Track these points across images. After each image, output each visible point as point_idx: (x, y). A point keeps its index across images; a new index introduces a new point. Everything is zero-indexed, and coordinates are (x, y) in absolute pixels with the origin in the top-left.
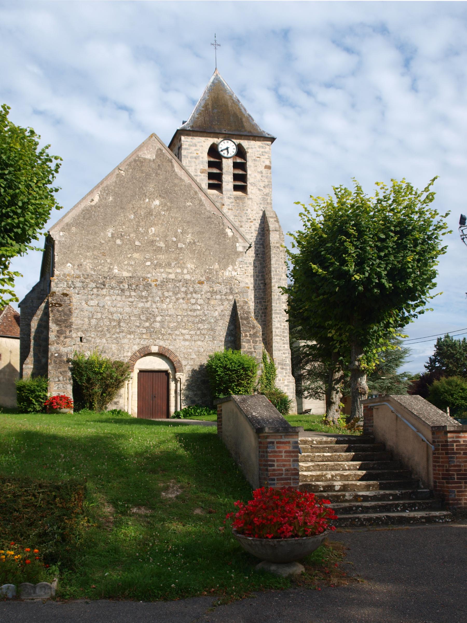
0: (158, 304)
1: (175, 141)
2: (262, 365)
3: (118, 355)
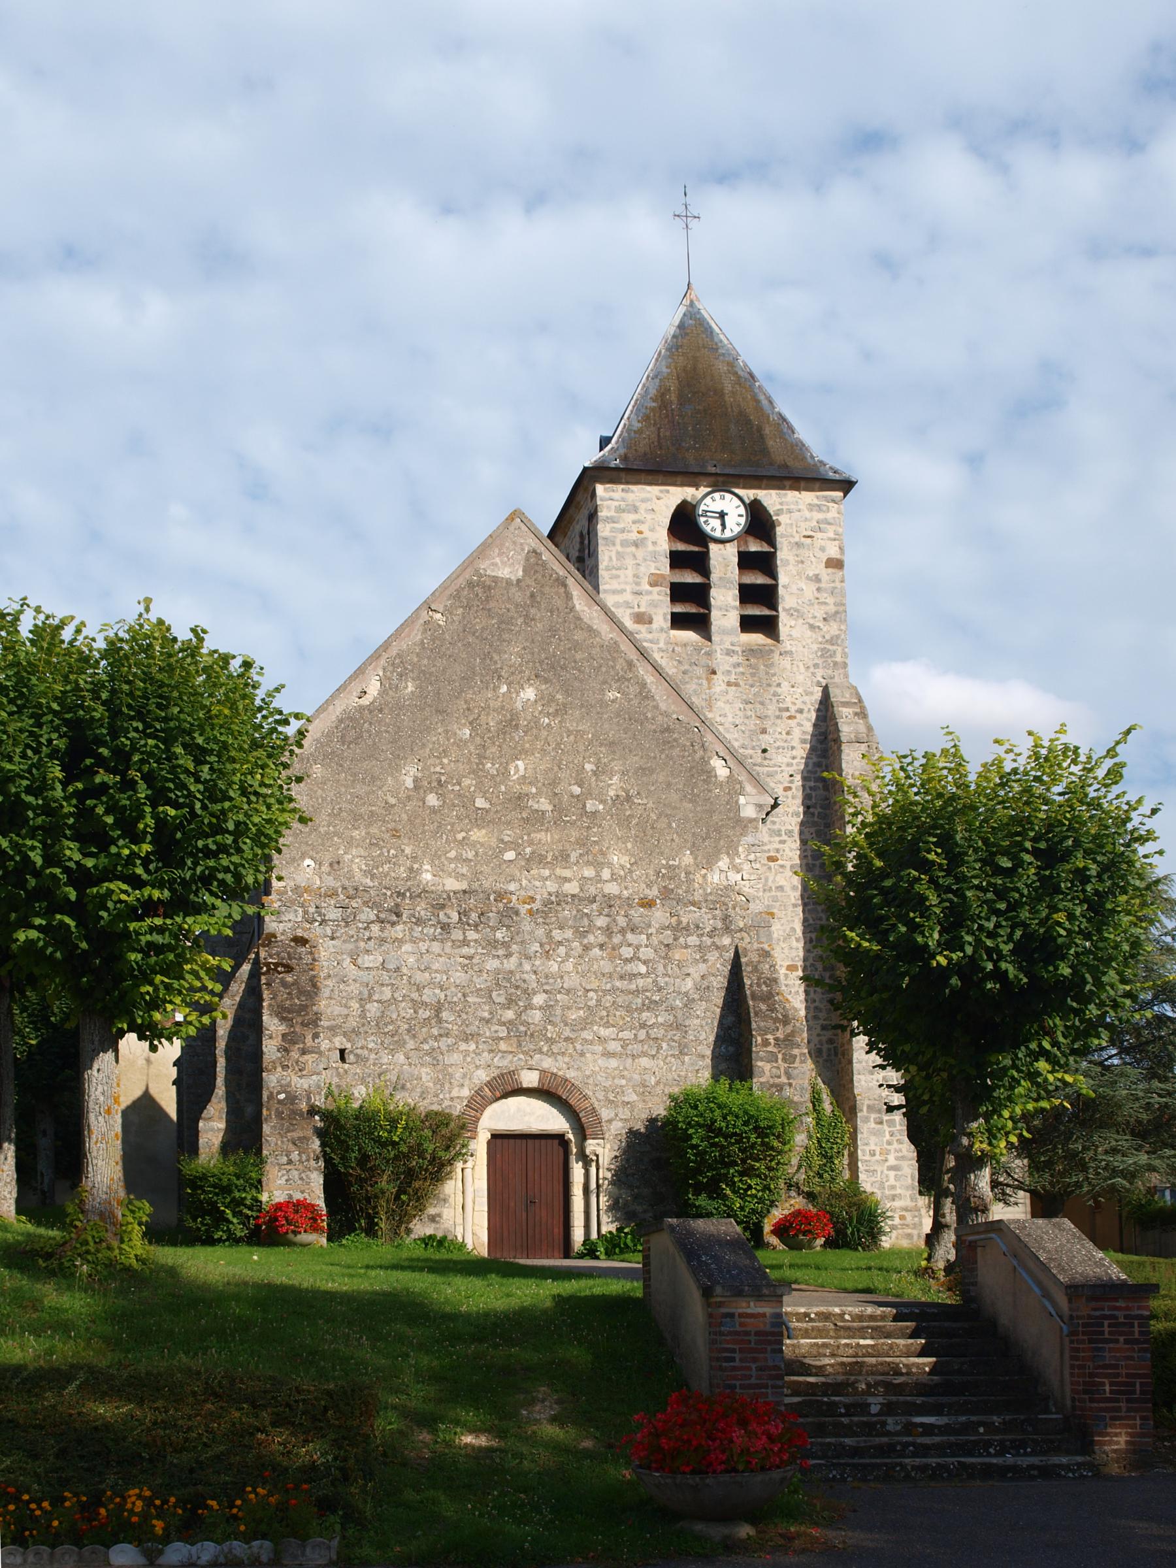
0: (537, 963)
1: (579, 497)
2: (810, 1120)
3: (437, 1096)
